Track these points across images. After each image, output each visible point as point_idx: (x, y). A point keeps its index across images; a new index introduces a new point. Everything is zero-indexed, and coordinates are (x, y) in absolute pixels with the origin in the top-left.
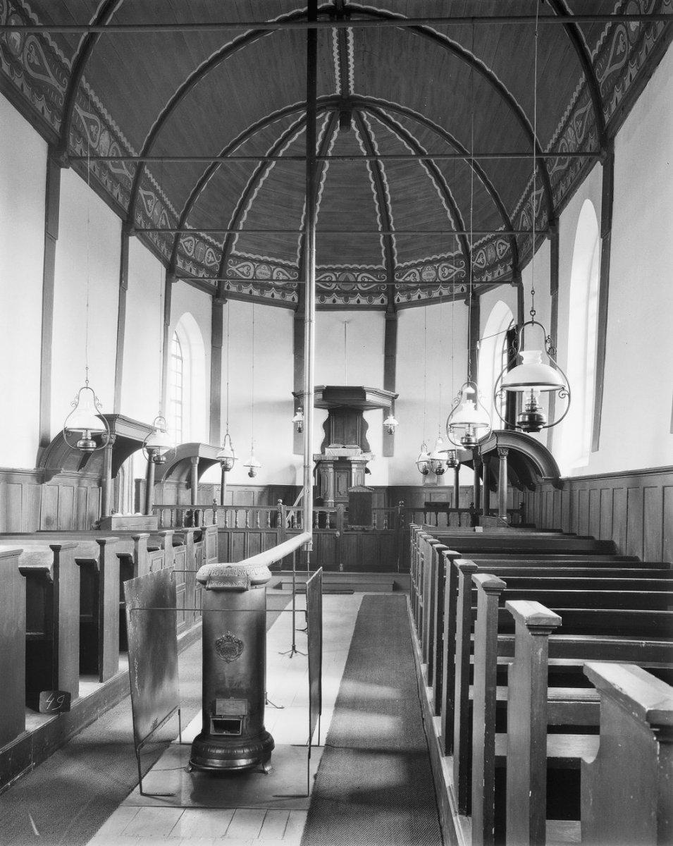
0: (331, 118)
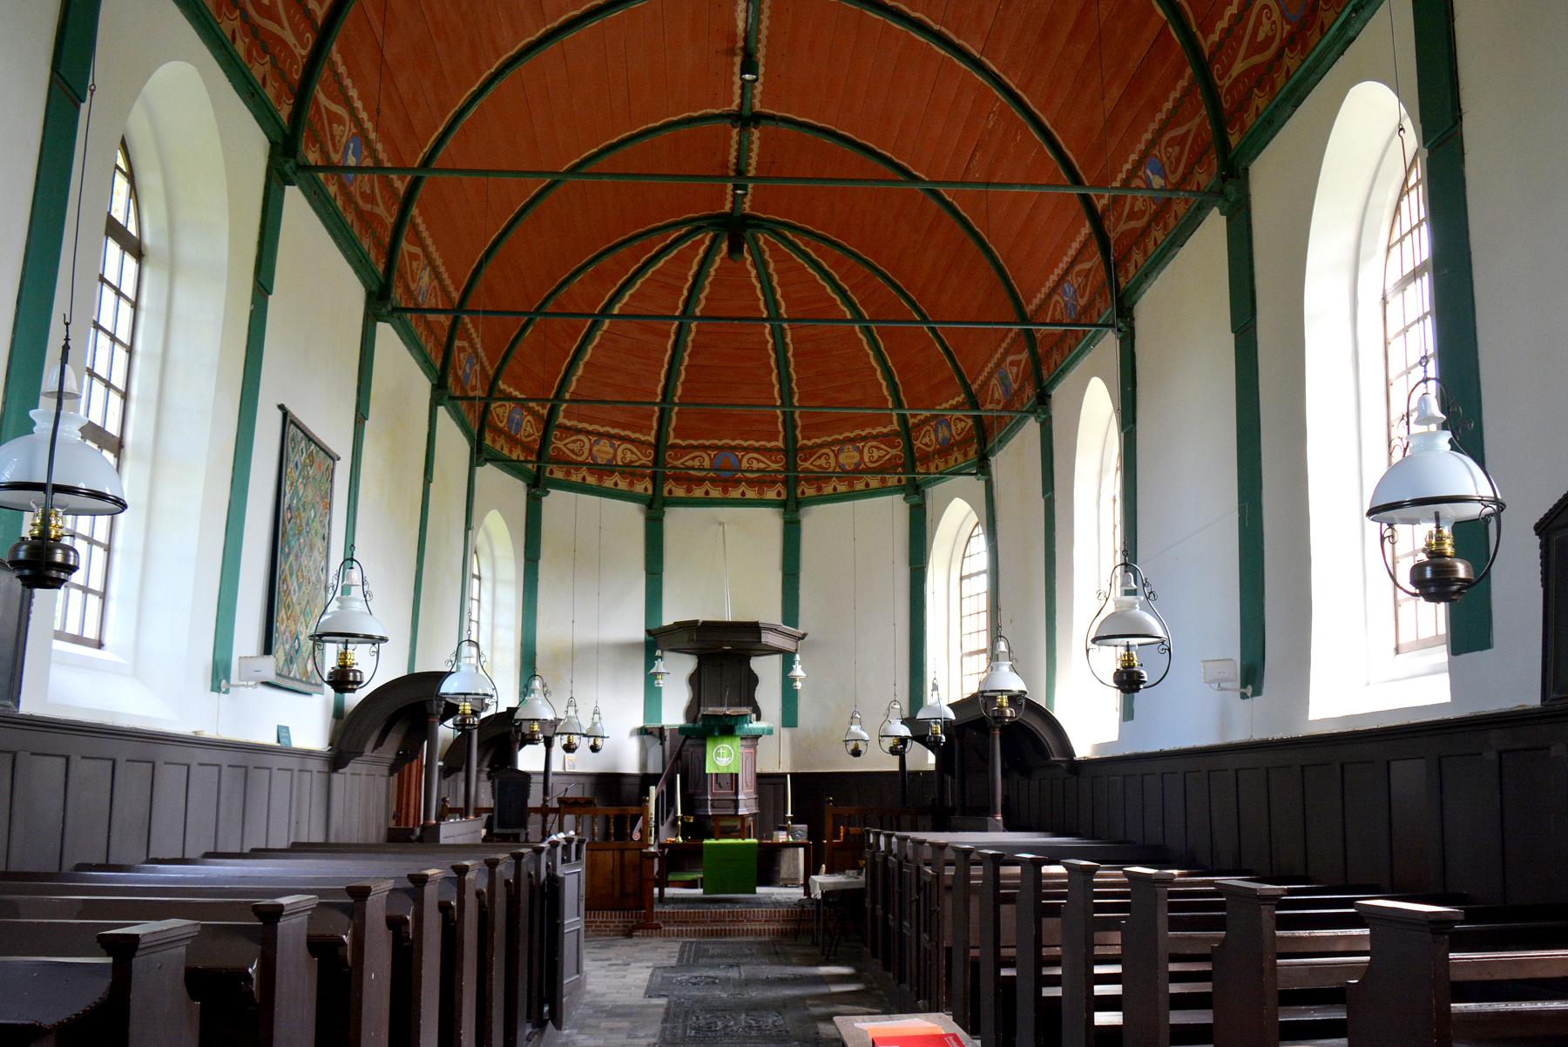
0: (713, 241)
